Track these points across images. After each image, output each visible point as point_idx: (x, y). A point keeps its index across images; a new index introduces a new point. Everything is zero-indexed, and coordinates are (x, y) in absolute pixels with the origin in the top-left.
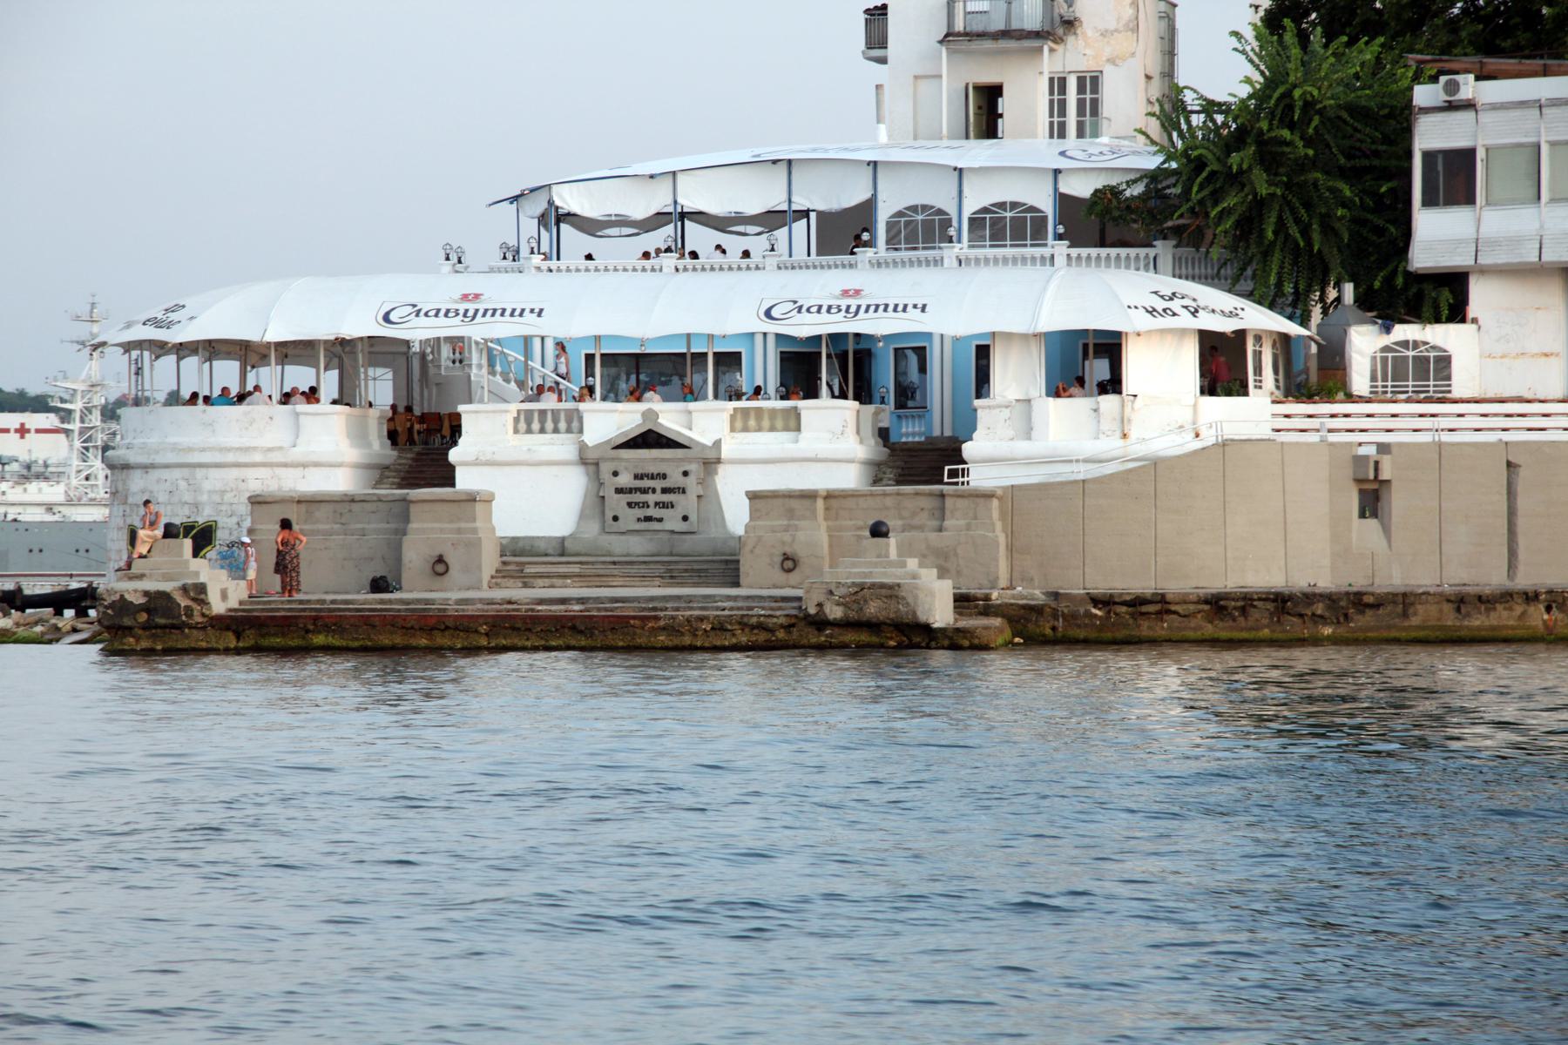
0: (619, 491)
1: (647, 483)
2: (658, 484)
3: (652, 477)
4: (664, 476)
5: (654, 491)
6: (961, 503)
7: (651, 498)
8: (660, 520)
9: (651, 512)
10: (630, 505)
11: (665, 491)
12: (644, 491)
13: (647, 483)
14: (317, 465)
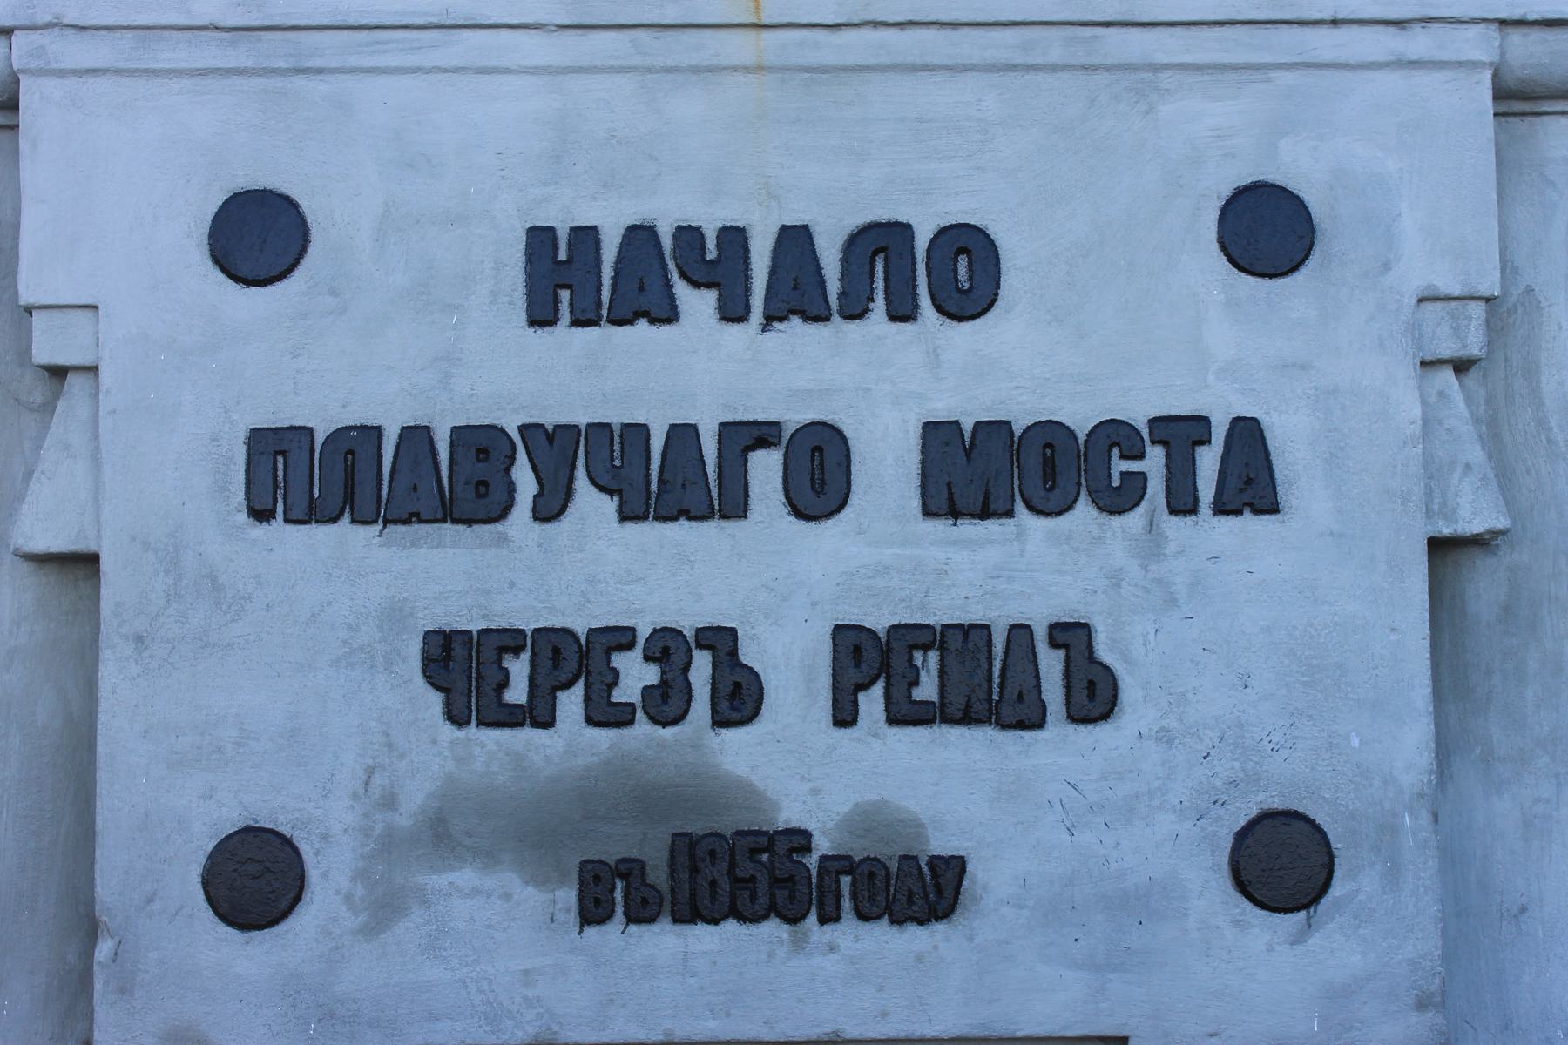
0: (310, 476)
1: (693, 370)
2: (886, 381)
3: (798, 285)
4: (961, 271)
5: (820, 472)
6: (50, 85)
7: (777, 583)
8: (919, 888)
9: (807, 769)
10: (464, 670)
11: (980, 471)
12: (672, 479)
13: (693, 370)
14: (747, 69)
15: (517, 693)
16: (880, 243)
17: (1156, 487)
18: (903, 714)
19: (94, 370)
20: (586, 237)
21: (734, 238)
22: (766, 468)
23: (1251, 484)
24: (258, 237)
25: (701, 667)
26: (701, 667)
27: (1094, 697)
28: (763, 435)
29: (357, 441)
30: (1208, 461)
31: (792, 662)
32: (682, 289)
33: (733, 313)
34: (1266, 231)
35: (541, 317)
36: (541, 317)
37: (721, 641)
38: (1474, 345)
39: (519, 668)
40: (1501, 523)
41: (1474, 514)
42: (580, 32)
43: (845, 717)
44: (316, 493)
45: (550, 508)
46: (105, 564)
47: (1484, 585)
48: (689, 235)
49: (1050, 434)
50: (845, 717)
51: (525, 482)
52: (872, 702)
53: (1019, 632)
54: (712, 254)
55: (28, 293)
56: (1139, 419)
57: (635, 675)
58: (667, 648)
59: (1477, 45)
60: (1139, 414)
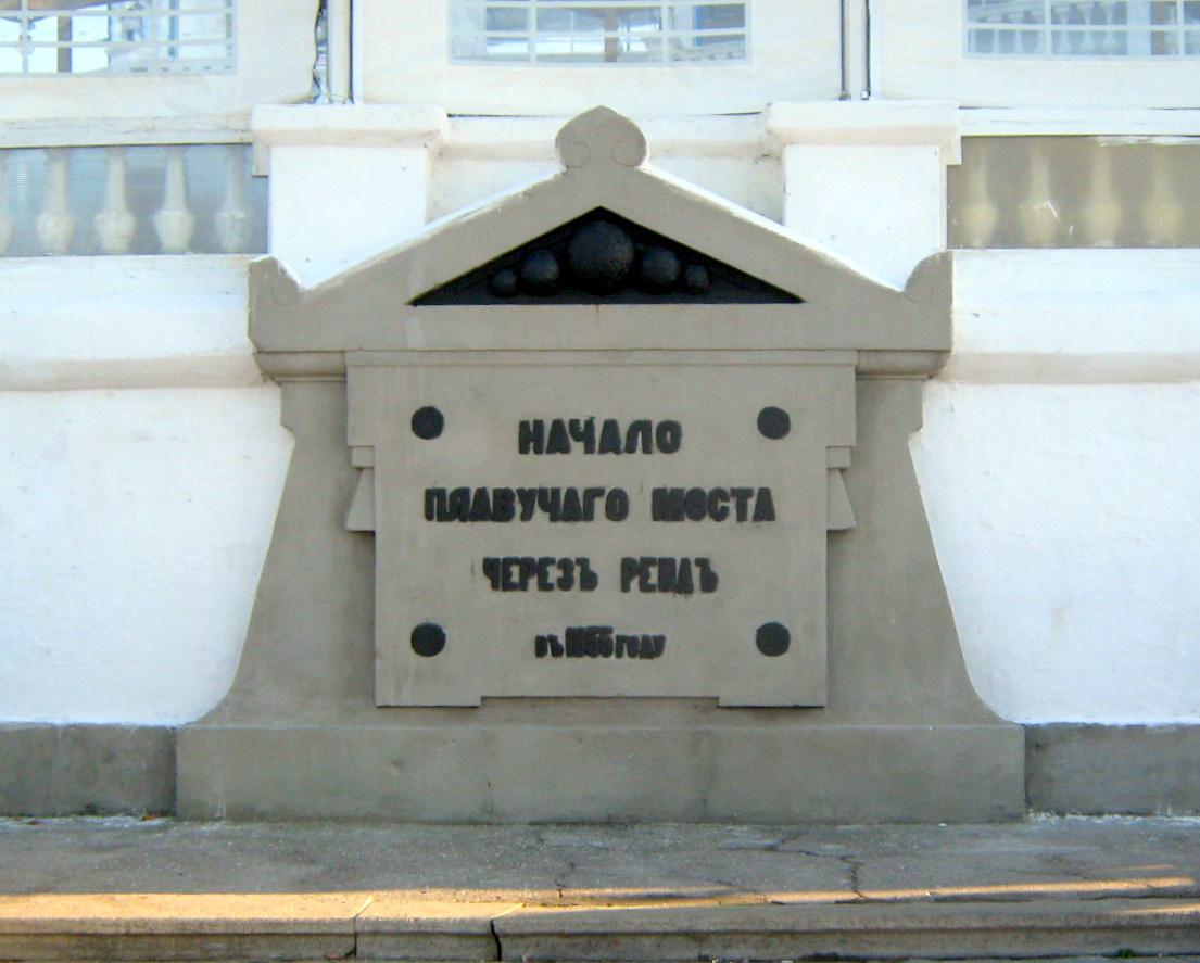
0: (448, 506)
1: (573, 470)
2: (641, 474)
3: (610, 440)
4: (668, 437)
5: (618, 506)
8: (650, 648)
9: (610, 607)
10: (497, 572)
11: (672, 505)
12: (568, 507)
13: (573, 470)
15: (515, 578)
16: (641, 427)
17: (733, 512)
18: (645, 587)
19: (372, 468)
20: (539, 424)
21: (590, 424)
22: (600, 504)
23: (766, 511)
24: (428, 423)
25: (577, 571)
26: (577, 571)
27: (710, 582)
28: (598, 492)
29: (462, 493)
30: (752, 503)
31: (607, 571)
32: (571, 440)
33: (589, 450)
34: (774, 423)
35: (523, 450)
36: (523, 450)
37: (583, 562)
38: (846, 462)
39: (515, 570)
40: (853, 524)
41: (845, 520)
42: (846, 8)
43: (625, 588)
44: (913, 961)
45: (526, 516)
46: (377, 534)
47: (850, 547)
48: (574, 423)
49: (696, 493)
50: (625, 588)
51: (518, 508)
52: (635, 583)
53: (685, 562)
54: (532, 444)
55: (351, 442)
56: (728, 490)
57: (554, 574)
58: (566, 565)
59: (853, 358)
60: (727, 487)
